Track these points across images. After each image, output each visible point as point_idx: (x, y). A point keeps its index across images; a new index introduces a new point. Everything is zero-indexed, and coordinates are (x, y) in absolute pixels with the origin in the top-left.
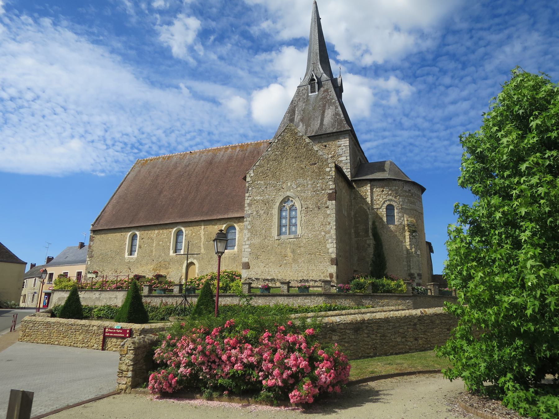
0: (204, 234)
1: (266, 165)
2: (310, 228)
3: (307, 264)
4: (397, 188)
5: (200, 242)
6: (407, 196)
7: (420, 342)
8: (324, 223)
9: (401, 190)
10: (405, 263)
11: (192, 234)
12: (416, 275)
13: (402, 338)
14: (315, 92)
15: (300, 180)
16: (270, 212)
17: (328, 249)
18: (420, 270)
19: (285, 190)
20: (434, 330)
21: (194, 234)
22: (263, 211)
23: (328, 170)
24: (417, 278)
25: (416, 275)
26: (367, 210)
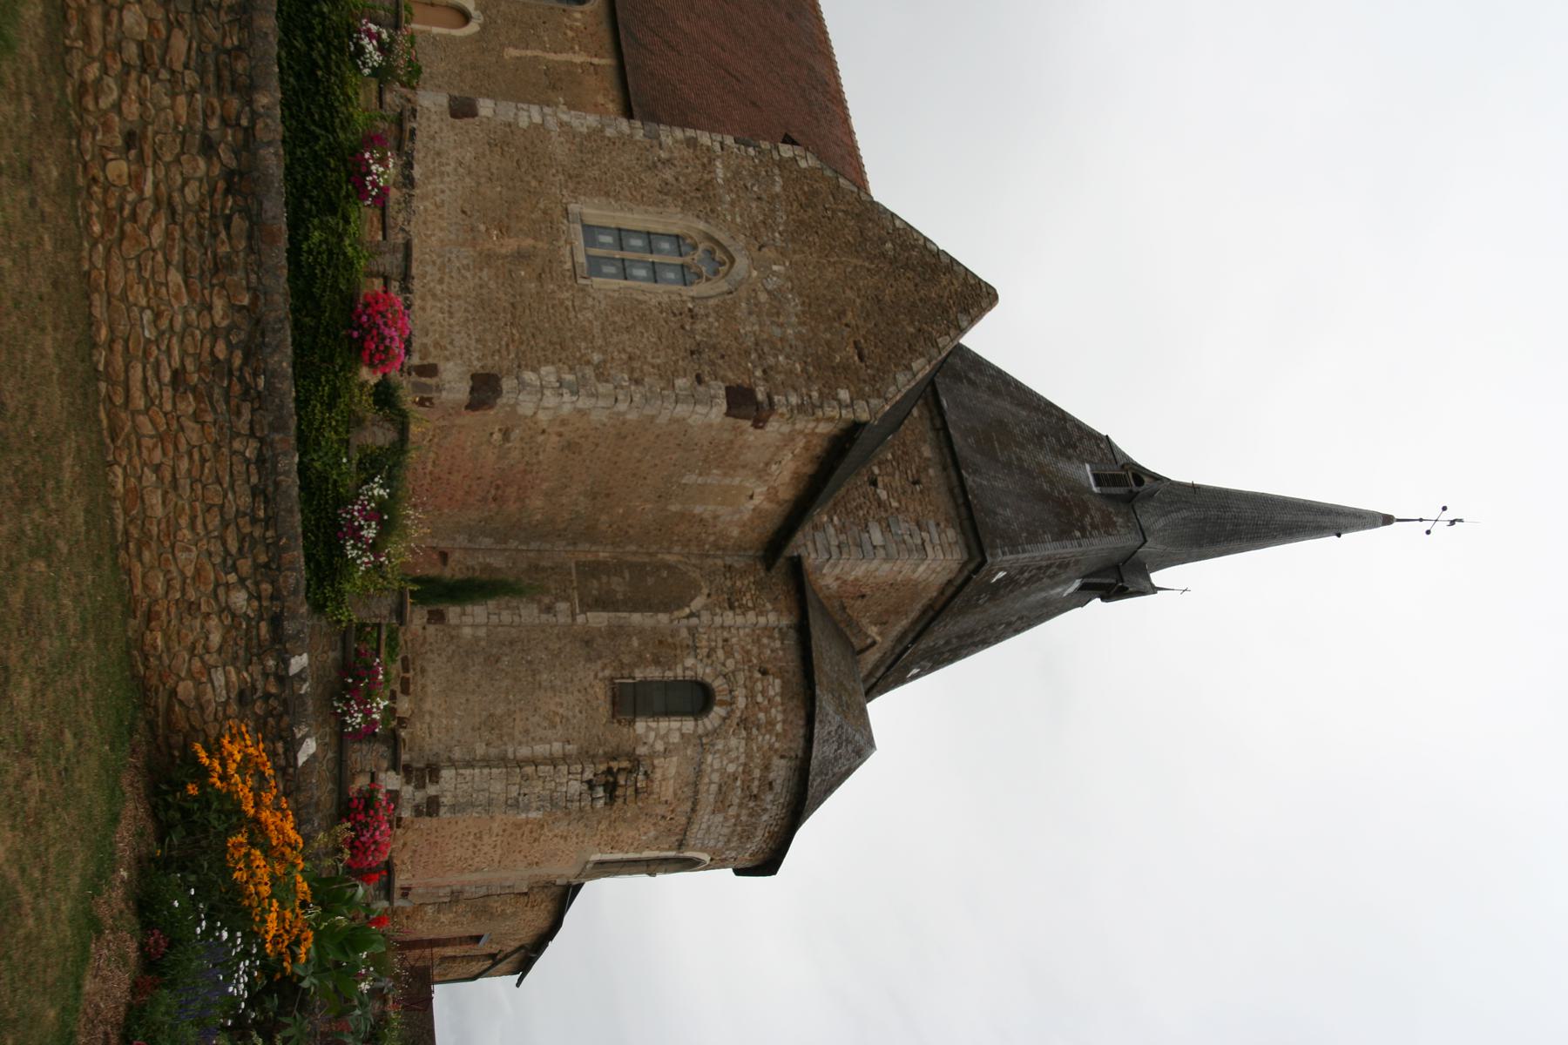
0: (572, 64)
1: (842, 207)
2: (617, 319)
3: (473, 294)
4: (779, 727)
5: (544, 49)
6: (747, 771)
7: (118, 168)
8: (636, 364)
9: (771, 747)
10: (480, 749)
11: (571, 29)
12: (432, 790)
13: (140, 44)
14: (1098, 484)
15: (794, 305)
16: (669, 199)
17: (535, 370)
18: (453, 808)
19: (755, 254)
20: (175, 277)
21: (570, 34)
22: (671, 180)
23: (844, 395)
24: (420, 796)
25: (432, 790)
26: (687, 611)
